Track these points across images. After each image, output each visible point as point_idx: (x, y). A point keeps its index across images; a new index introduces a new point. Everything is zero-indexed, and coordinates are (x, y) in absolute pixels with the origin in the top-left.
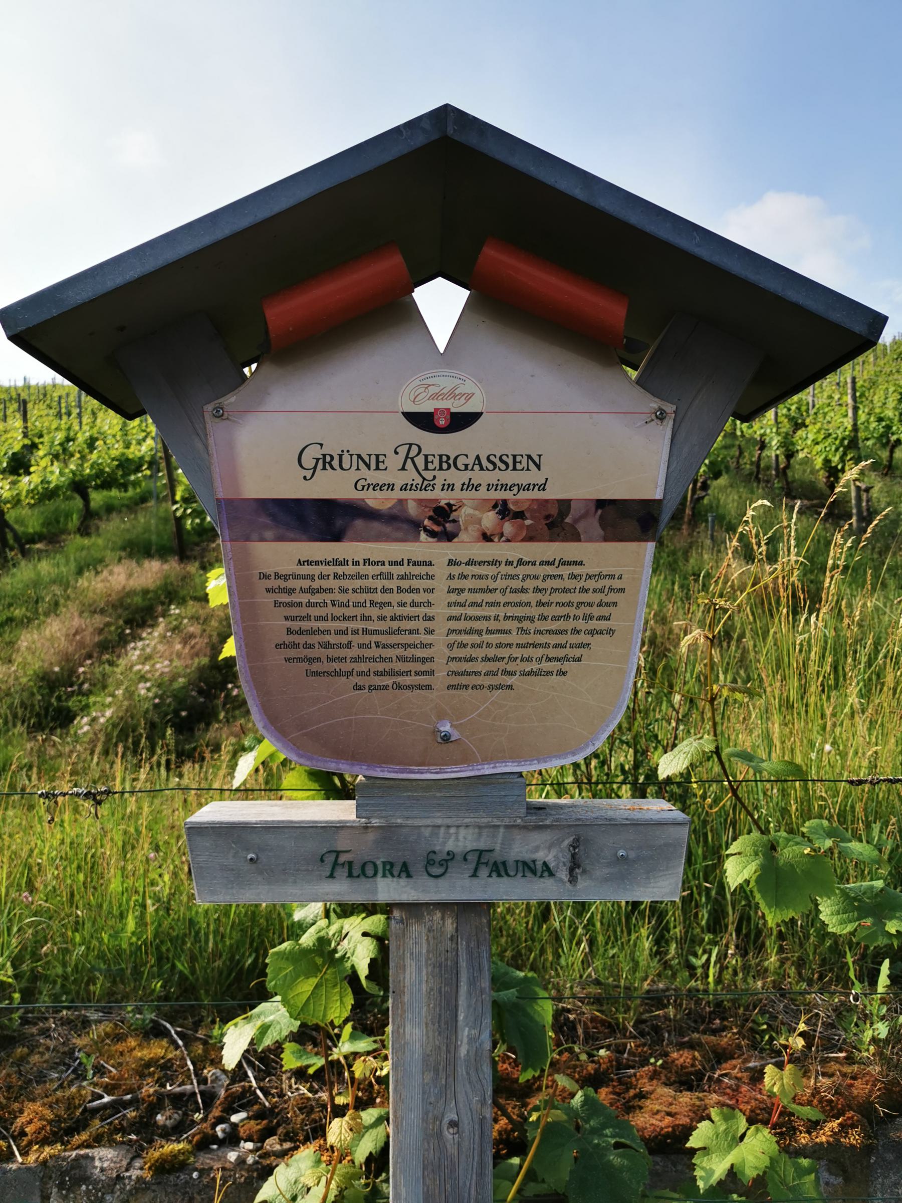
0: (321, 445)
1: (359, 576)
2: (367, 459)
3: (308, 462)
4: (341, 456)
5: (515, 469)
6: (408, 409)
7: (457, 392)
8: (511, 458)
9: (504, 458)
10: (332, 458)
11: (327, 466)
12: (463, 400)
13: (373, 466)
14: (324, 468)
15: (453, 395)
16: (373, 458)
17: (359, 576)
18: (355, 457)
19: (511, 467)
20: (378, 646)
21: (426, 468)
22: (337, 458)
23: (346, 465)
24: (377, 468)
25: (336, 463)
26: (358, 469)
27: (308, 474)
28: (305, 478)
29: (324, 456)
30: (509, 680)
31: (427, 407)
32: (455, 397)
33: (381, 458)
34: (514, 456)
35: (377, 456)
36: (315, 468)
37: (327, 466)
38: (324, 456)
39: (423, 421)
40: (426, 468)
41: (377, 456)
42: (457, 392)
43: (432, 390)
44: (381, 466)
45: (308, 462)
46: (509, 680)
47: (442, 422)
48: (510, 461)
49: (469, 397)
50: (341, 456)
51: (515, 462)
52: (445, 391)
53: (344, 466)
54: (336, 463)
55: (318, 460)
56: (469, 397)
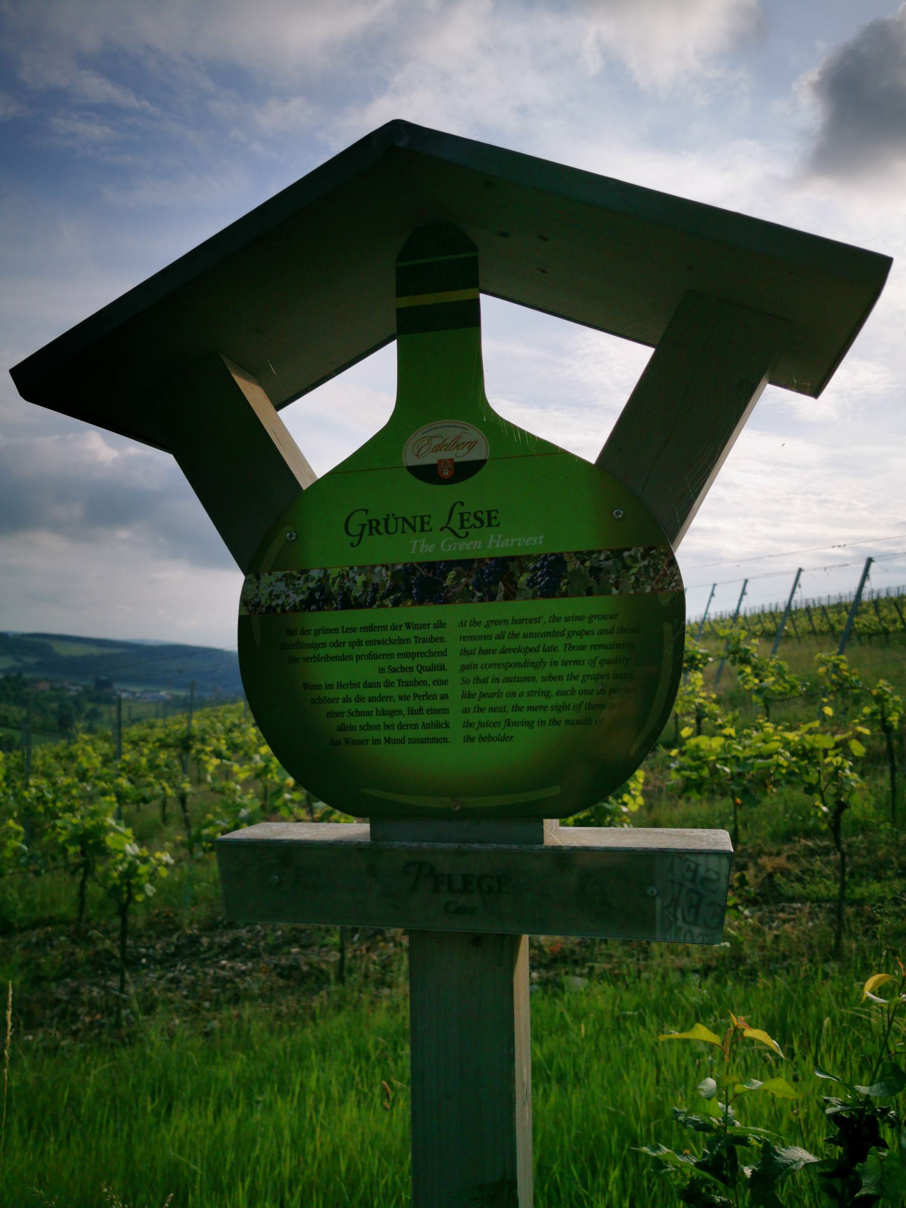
0: (367, 511)
1: (401, 641)
2: (411, 520)
3: (355, 528)
4: (386, 520)
5: (490, 525)
6: (410, 464)
7: (460, 441)
8: (486, 514)
9: (479, 515)
10: (378, 523)
11: (374, 530)
12: (466, 449)
13: (418, 527)
14: (371, 534)
15: (456, 444)
16: (418, 520)
17: (401, 641)
18: (400, 521)
19: (486, 523)
20: (347, 743)
21: (462, 527)
22: (382, 523)
23: (392, 528)
24: (423, 530)
25: (382, 528)
26: (403, 532)
27: (355, 540)
28: (352, 545)
29: (370, 521)
30: (509, 731)
31: (431, 459)
32: (457, 447)
33: (426, 519)
34: (489, 513)
35: (422, 517)
36: (361, 534)
37: (374, 530)
38: (370, 521)
39: (427, 474)
40: (462, 527)
41: (422, 517)
42: (460, 441)
43: (436, 442)
44: (427, 527)
45: (355, 528)
46: (509, 731)
47: (446, 473)
48: (485, 518)
49: (472, 445)
50: (386, 520)
51: (490, 518)
52: (448, 442)
53: (350, 531)
54: (382, 528)
55: (364, 526)
56: (472, 445)
